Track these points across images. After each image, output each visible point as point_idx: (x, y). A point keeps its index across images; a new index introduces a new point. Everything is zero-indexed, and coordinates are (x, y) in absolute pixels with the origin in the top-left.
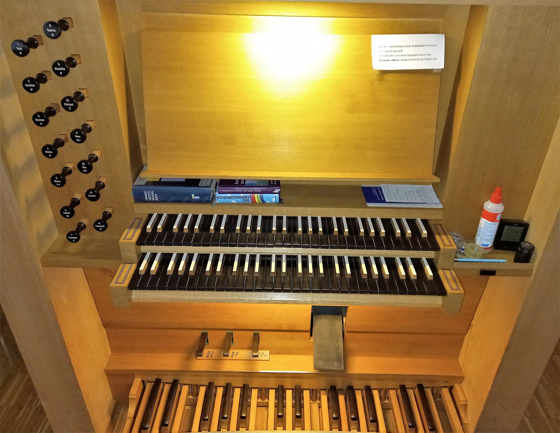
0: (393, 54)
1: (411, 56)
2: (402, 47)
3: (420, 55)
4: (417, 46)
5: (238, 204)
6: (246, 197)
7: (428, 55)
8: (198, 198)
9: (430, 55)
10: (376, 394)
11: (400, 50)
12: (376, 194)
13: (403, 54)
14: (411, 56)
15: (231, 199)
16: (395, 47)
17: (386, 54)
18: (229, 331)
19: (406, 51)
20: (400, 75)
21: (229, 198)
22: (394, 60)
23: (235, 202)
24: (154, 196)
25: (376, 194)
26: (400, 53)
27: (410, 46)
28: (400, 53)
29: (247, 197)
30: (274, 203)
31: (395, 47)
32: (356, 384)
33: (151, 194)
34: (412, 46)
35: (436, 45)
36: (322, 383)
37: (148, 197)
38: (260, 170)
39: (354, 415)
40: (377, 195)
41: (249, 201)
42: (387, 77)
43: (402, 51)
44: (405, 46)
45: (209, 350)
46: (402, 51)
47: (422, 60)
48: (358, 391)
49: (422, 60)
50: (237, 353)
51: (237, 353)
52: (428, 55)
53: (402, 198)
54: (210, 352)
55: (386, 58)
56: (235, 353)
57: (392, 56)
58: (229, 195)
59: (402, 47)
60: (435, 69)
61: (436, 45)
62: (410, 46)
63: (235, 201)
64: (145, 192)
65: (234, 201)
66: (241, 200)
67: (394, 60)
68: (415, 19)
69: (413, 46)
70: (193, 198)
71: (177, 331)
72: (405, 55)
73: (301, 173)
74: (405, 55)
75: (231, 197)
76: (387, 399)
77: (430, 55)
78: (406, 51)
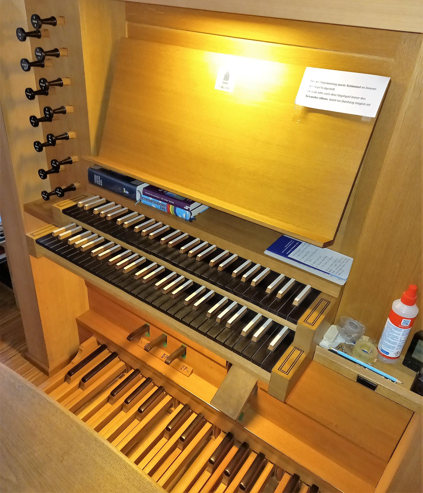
0: (324, 91)
1: (342, 96)
2: (336, 85)
3: (352, 97)
4: (353, 87)
5: (156, 209)
6: (163, 205)
7: (362, 98)
8: (127, 193)
9: (365, 99)
10: (269, 467)
11: (332, 88)
12: (286, 247)
13: (334, 94)
14: (342, 96)
15: (152, 202)
16: (328, 84)
17: (316, 90)
18: (184, 345)
19: (339, 90)
20: (326, 116)
21: (150, 202)
22: (322, 98)
23: (155, 207)
24: (100, 181)
25: (286, 247)
26: (331, 92)
27: (344, 85)
28: (331, 92)
29: (164, 206)
30: (184, 219)
31: (328, 84)
32: (253, 445)
33: (98, 178)
34: (346, 85)
35: (375, 89)
36: (229, 427)
37: (96, 180)
38: (154, 175)
39: (214, 459)
40: (286, 249)
41: (165, 210)
42: (312, 116)
43: (334, 89)
44: (339, 85)
45: (165, 352)
46: (334, 89)
47: (353, 103)
48: (255, 453)
49: (353, 103)
50: (186, 368)
51: (186, 368)
52: (362, 98)
53: (310, 259)
54: (165, 354)
55: (314, 95)
56: (185, 367)
57: (321, 93)
58: (151, 199)
59: (336, 85)
60: (363, 116)
61: (375, 89)
62: (344, 85)
63: (155, 206)
64: (95, 176)
65: (153, 206)
66: (159, 207)
67: (322, 98)
68: (361, 56)
69: (348, 86)
70: (124, 192)
71: (142, 320)
72: (335, 95)
73: (255, 214)
74: (335, 95)
75: (151, 201)
76: (275, 475)
77: (365, 99)
78: (339, 90)
